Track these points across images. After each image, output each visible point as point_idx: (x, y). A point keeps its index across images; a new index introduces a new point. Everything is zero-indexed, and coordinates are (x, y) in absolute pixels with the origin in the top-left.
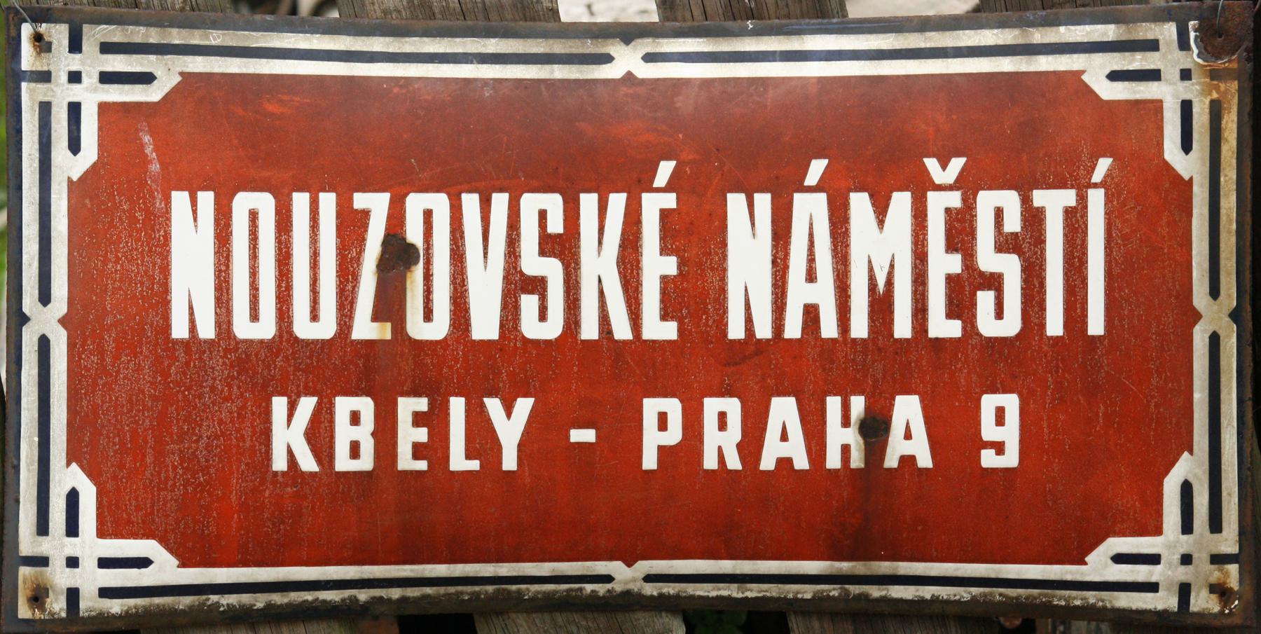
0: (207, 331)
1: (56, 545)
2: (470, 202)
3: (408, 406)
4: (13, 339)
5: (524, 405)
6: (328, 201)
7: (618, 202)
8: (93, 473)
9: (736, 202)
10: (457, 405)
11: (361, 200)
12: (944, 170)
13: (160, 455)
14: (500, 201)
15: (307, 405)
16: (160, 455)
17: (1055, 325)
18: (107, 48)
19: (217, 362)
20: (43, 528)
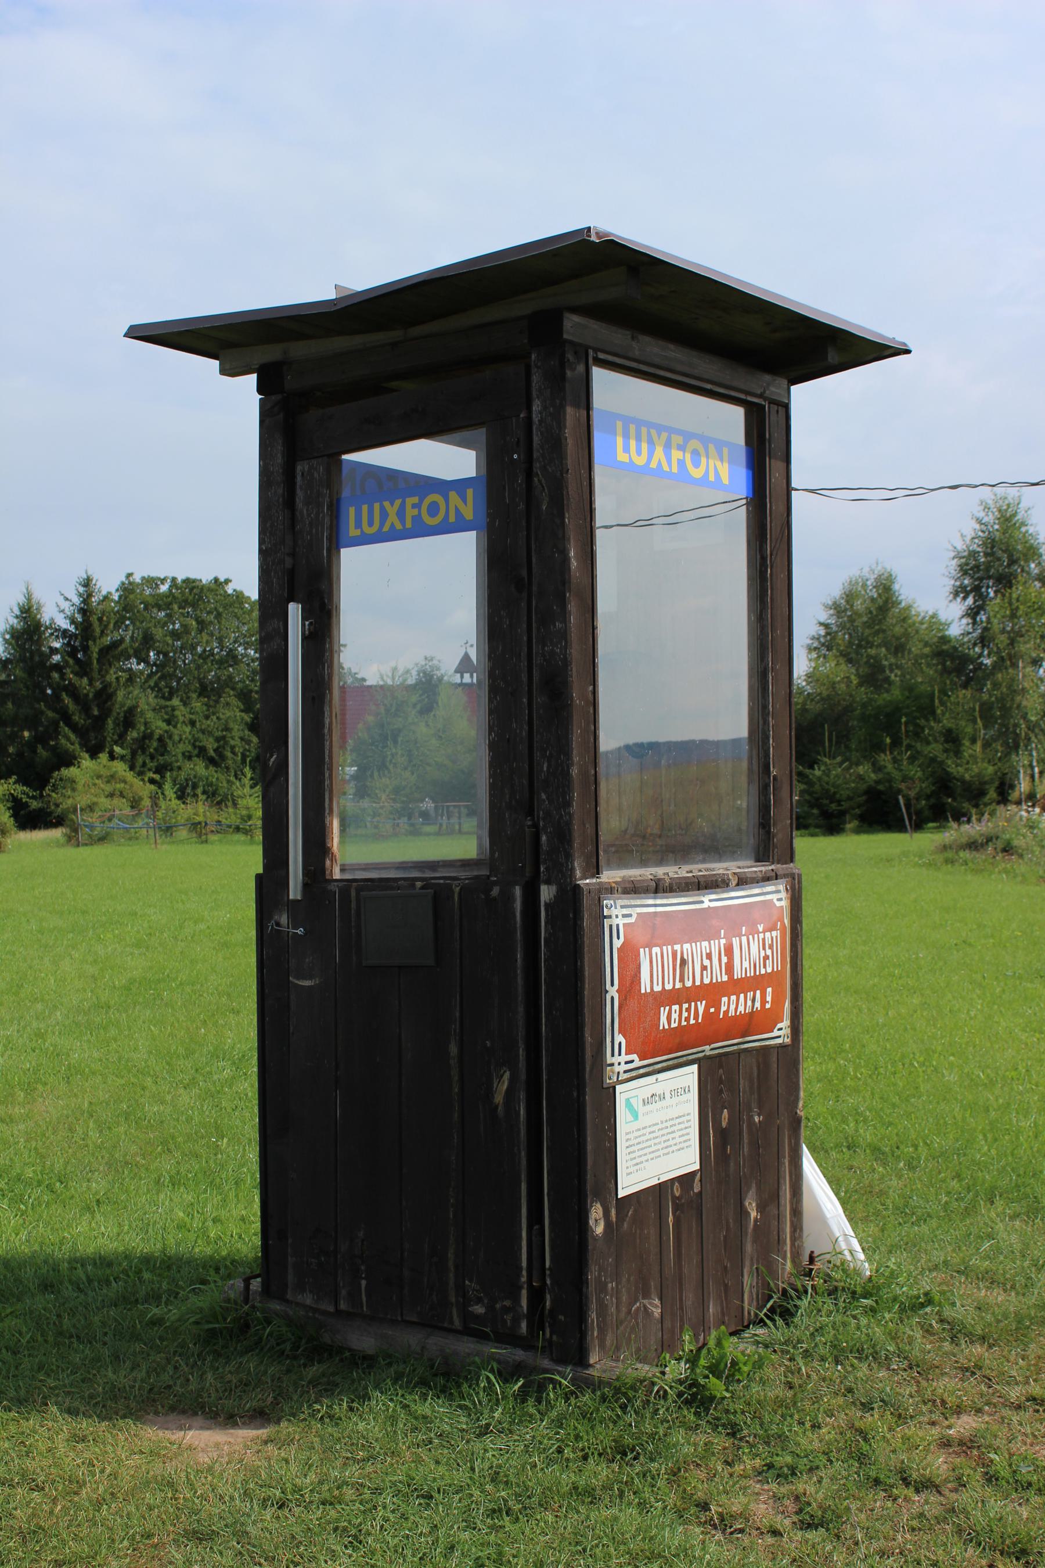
0: (648, 990)
1: (616, 1059)
2: (694, 944)
3: (686, 1006)
4: (774, 467)
5: (704, 1002)
6: (669, 947)
7: (717, 941)
8: (624, 1036)
9: (734, 939)
10: (693, 1004)
11: (685, 1023)
12: (126, 335)
13: (639, 1028)
14: (698, 943)
15: (667, 1008)
16: (639, 1028)
17: (365, 508)
18: (622, 907)
19: (650, 999)
20: (613, 1055)
